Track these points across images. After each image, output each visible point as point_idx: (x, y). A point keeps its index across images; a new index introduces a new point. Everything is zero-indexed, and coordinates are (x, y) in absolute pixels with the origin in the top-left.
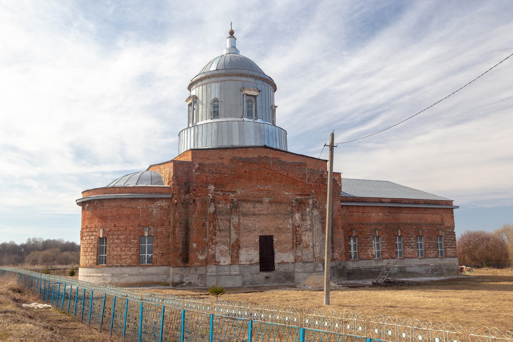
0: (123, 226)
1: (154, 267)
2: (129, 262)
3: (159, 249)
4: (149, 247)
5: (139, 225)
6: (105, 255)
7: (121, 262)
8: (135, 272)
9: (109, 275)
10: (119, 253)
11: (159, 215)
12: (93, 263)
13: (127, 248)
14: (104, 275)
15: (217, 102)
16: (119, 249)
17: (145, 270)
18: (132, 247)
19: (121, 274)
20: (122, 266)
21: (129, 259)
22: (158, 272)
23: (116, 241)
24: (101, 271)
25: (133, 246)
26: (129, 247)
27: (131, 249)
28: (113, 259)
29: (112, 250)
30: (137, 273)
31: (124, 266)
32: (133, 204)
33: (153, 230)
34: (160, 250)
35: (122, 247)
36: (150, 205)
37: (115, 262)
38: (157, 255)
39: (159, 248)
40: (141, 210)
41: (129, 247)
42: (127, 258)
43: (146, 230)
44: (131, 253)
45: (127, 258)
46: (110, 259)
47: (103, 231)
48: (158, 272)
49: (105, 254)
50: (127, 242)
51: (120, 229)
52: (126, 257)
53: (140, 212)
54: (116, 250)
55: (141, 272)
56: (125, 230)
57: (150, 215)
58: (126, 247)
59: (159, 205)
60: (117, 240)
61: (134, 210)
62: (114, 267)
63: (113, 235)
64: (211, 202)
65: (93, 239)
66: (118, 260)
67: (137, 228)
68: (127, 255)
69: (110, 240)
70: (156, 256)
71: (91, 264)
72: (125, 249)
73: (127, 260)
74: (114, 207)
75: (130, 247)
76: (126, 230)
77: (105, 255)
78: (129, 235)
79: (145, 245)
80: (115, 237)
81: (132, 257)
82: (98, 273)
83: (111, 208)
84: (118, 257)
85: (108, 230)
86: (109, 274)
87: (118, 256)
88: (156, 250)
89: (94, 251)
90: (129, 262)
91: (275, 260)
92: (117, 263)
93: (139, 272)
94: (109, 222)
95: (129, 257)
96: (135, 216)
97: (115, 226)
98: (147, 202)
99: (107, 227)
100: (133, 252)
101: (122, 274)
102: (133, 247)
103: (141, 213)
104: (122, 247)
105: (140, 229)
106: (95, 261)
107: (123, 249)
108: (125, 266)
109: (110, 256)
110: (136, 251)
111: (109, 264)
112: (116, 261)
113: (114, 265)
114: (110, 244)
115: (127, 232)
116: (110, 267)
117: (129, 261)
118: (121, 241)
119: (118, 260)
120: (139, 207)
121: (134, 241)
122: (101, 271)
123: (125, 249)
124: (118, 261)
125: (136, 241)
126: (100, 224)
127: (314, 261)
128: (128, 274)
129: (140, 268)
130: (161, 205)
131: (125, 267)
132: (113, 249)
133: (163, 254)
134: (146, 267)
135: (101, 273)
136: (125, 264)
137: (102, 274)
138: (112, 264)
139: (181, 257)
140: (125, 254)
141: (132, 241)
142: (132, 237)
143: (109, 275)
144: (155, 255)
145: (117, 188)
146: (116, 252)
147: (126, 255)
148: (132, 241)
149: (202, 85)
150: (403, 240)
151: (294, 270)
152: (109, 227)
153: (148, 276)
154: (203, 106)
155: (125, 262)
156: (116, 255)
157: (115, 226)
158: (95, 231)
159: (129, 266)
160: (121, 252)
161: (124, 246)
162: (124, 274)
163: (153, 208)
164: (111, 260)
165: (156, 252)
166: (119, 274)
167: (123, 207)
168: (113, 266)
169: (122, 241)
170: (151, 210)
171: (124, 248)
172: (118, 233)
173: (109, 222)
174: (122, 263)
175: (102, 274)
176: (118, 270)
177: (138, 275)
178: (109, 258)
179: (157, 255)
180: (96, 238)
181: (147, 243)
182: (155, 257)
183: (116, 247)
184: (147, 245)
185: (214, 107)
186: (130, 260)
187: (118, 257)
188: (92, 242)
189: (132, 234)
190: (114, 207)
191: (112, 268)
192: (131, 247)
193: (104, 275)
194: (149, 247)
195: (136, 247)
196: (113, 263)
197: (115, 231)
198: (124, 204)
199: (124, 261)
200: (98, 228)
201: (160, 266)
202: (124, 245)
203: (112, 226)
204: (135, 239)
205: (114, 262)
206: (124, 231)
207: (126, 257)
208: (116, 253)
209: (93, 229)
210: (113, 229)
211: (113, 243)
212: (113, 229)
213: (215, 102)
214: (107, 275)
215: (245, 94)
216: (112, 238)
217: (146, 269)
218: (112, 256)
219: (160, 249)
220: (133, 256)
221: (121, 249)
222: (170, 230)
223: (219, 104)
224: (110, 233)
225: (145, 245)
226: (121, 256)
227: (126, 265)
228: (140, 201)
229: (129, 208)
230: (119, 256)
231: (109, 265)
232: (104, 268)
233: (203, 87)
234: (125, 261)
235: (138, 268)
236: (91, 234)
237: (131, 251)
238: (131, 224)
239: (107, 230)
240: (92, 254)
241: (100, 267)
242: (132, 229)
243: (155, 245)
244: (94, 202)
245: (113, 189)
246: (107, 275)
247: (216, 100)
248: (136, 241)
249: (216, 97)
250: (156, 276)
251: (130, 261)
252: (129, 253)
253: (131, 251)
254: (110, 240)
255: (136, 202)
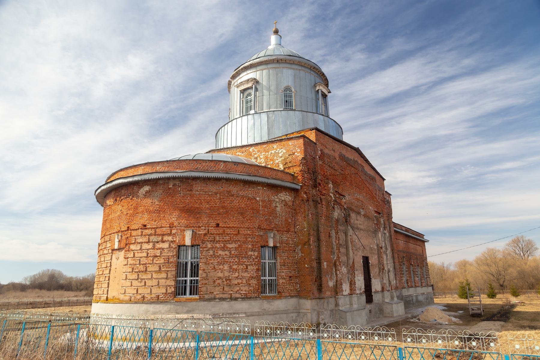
0: (233, 227)
1: (283, 300)
2: (245, 291)
3: (286, 269)
4: (270, 265)
5: (259, 228)
6: (269, 278)
7: (231, 291)
8: (256, 310)
9: (208, 316)
10: (227, 274)
11: (284, 214)
12: (166, 294)
13: (242, 265)
14: (195, 316)
15: (290, 91)
16: (226, 267)
17: (271, 305)
18: (249, 265)
19: (231, 314)
20: (231, 299)
21: (245, 286)
22: (287, 307)
23: (220, 252)
24: (187, 309)
25: (251, 262)
26: (245, 265)
27: (249, 267)
28: (215, 286)
29: (212, 269)
30: (259, 310)
31: (236, 299)
32: (249, 192)
33: (278, 237)
34: (288, 271)
35: (231, 264)
36: (273, 197)
37: (218, 291)
38: (285, 279)
39: (287, 267)
40: (261, 203)
41: (245, 265)
42: (242, 283)
43: (271, 236)
44: (249, 275)
45: (242, 283)
46: (207, 286)
47: (192, 234)
48: (287, 307)
49: (269, 276)
50: (241, 254)
51: (228, 231)
52: (240, 281)
53: (260, 205)
54: (220, 269)
55: (265, 310)
56: (236, 235)
57: (273, 212)
58: (239, 264)
59: (283, 198)
60: (223, 251)
61: (252, 203)
62: (217, 300)
63: (214, 241)
64: (334, 204)
65: (163, 249)
66: (225, 287)
67: (256, 233)
68: (241, 278)
69: (207, 251)
70: (284, 281)
71: (159, 296)
72: (238, 268)
73: (242, 288)
74: (216, 194)
75: (246, 263)
76: (239, 233)
77: (269, 278)
78: (245, 242)
79: (264, 261)
80: (218, 245)
81: (250, 282)
82: (178, 313)
83: (209, 195)
84: (225, 283)
85: (204, 232)
86: (207, 314)
87: (224, 280)
88: (283, 271)
89: (168, 271)
90: (245, 291)
91: (372, 288)
92: (224, 293)
93: (263, 308)
94: (205, 220)
95: (244, 282)
96: (253, 213)
97: (218, 225)
98: (269, 192)
99: (199, 227)
100: (252, 273)
101: (234, 314)
102: (252, 265)
103: (261, 207)
104: (231, 264)
105: (262, 233)
106: (171, 290)
107: (235, 267)
108: (238, 298)
109: (208, 279)
110: (255, 272)
111: (206, 294)
112: (222, 290)
113: (217, 296)
114: (207, 259)
115: (241, 238)
116: (209, 300)
117: (245, 289)
118: (230, 253)
119: (224, 288)
120: (258, 198)
121: (252, 253)
122: (185, 309)
123: (238, 268)
124: (225, 289)
125: (256, 254)
126: (184, 222)
127: (390, 289)
128: (245, 313)
129: (264, 301)
130: (285, 199)
131: (240, 300)
132: (214, 267)
133: (290, 277)
134: (273, 299)
135: (188, 312)
136: (238, 295)
137: (191, 315)
138: (212, 296)
139: (316, 283)
140: (239, 276)
141: (250, 253)
142: (250, 246)
143: (208, 316)
144: (283, 279)
145: (222, 163)
146: (221, 272)
147: (241, 279)
148: (250, 253)
149: (269, 69)
150: (413, 268)
151: (383, 301)
152: (203, 228)
153: (275, 315)
154: (271, 93)
155: (238, 290)
156: (220, 278)
157: (218, 225)
158: (170, 234)
159: (246, 298)
160: (230, 272)
161: (236, 262)
162: (238, 313)
163: (277, 202)
164: (210, 288)
165: (283, 274)
166: (228, 314)
167: (233, 196)
168: (215, 299)
169: (233, 252)
170: (274, 205)
171: (237, 266)
172: (223, 238)
173: (205, 220)
174: (231, 292)
175: (191, 315)
176: (225, 306)
177: (262, 314)
178: (206, 284)
179: (285, 279)
180: (174, 247)
181: (267, 258)
182: (283, 282)
183: (219, 263)
184: (267, 261)
185: (286, 96)
186: (246, 287)
187: (225, 283)
188: (161, 254)
189: (250, 241)
190: (216, 194)
191: (212, 303)
192: (248, 263)
193: (195, 316)
194: (270, 265)
195: (257, 265)
196: (215, 293)
197: (217, 234)
198: (234, 190)
199: (236, 290)
200: (178, 228)
201: (289, 298)
202: (236, 260)
203: (212, 227)
204: (254, 251)
205: (217, 292)
206: (234, 235)
207: (240, 281)
208: (220, 274)
209: (166, 230)
210: (213, 230)
211: (214, 256)
212: (213, 230)
213: (286, 91)
214: (201, 316)
215: (321, 89)
216: (212, 248)
217: (272, 303)
218: (211, 281)
219: (288, 269)
220: (251, 281)
221: (230, 267)
222: (295, 239)
223: (292, 94)
224: (207, 238)
225: (264, 261)
226: (230, 280)
227: (240, 296)
228: (259, 188)
229: (243, 197)
230: (226, 280)
231: (206, 297)
232: (194, 303)
233: (270, 71)
234: (238, 288)
235: (261, 301)
236: (161, 238)
237: (248, 272)
238: (247, 225)
239: (200, 233)
240: (164, 275)
241: (184, 301)
242: (249, 232)
243: (282, 263)
244: (168, 183)
245: (212, 164)
246: (201, 316)
247: (287, 89)
248: (256, 254)
249: (289, 85)
250: (285, 315)
251: (246, 288)
252: (246, 274)
253: (248, 272)
254: (207, 251)
255: (253, 189)
